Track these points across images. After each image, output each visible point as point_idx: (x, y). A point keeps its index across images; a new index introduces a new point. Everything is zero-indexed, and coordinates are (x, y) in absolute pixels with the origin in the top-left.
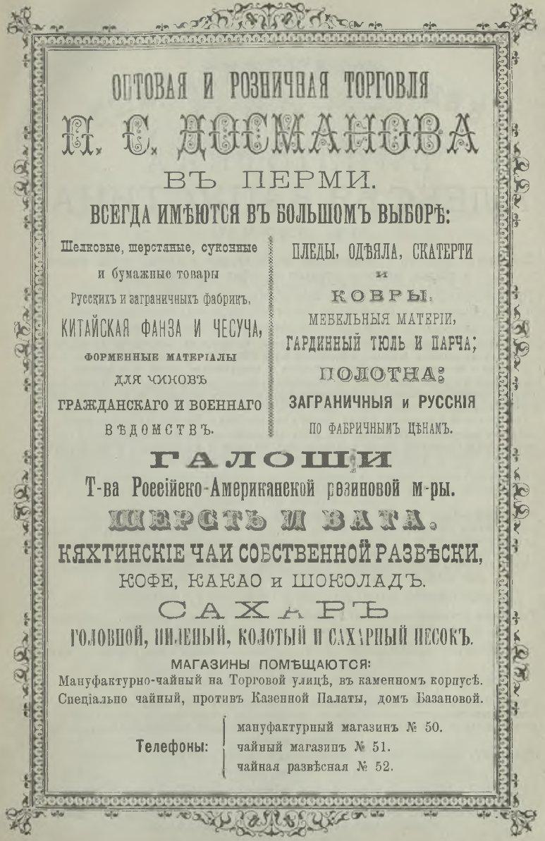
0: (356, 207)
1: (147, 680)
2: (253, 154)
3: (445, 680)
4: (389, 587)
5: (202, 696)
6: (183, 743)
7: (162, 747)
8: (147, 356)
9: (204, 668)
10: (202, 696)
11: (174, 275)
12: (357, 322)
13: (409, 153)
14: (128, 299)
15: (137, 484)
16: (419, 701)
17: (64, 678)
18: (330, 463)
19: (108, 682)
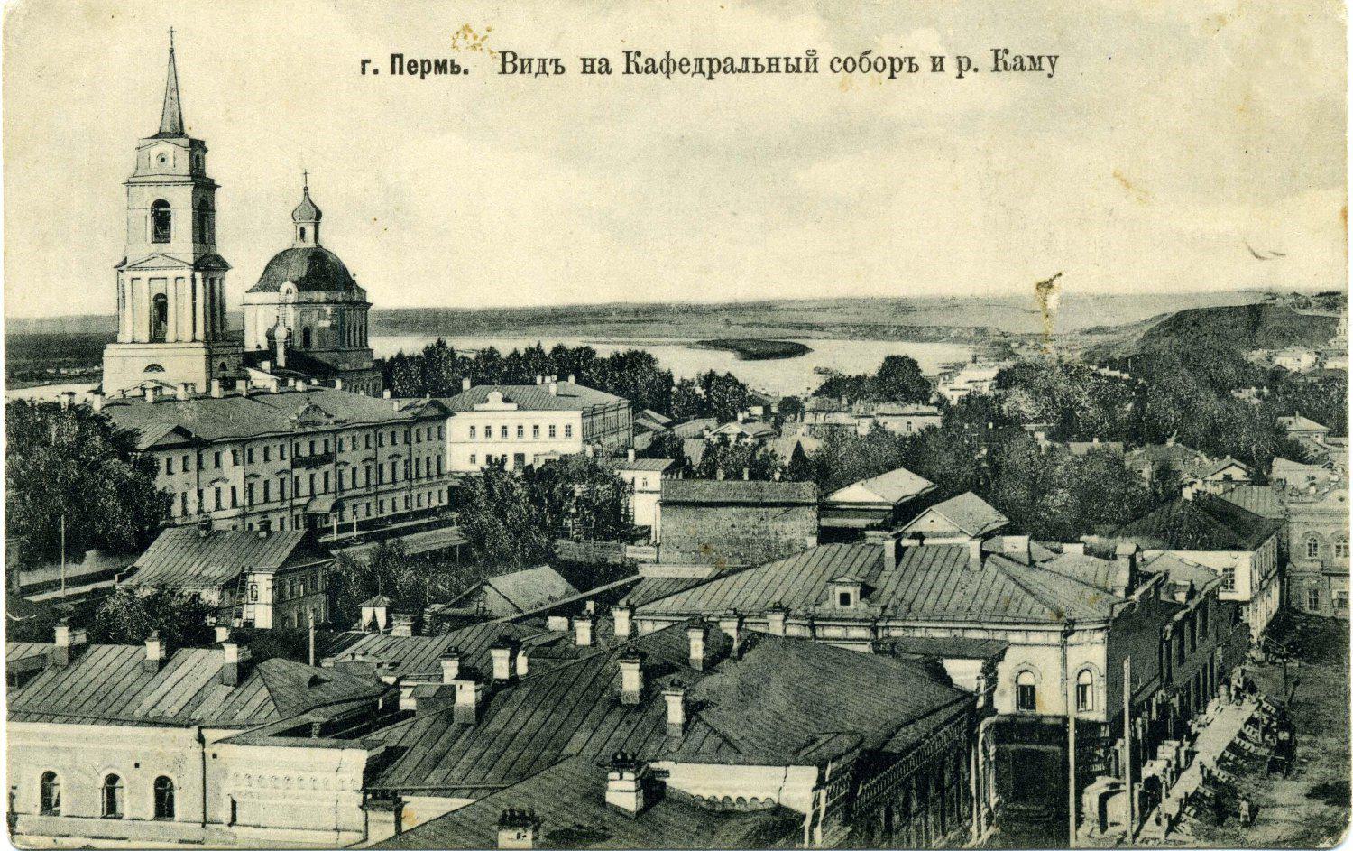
0: (547, 62)
1: (880, 67)
2: (829, 67)
3: (888, 63)
4: (536, 74)
5: (711, 60)
6: (411, 73)
7: (728, 66)
8: (766, 64)
9: (969, 75)
10: (711, 60)
11: (482, 65)
12: (760, 69)
13: (599, 58)
14: (535, 66)
15: (426, 70)
16: (504, 71)
17: (1036, 59)
18: (301, 495)
19: (1027, 62)
